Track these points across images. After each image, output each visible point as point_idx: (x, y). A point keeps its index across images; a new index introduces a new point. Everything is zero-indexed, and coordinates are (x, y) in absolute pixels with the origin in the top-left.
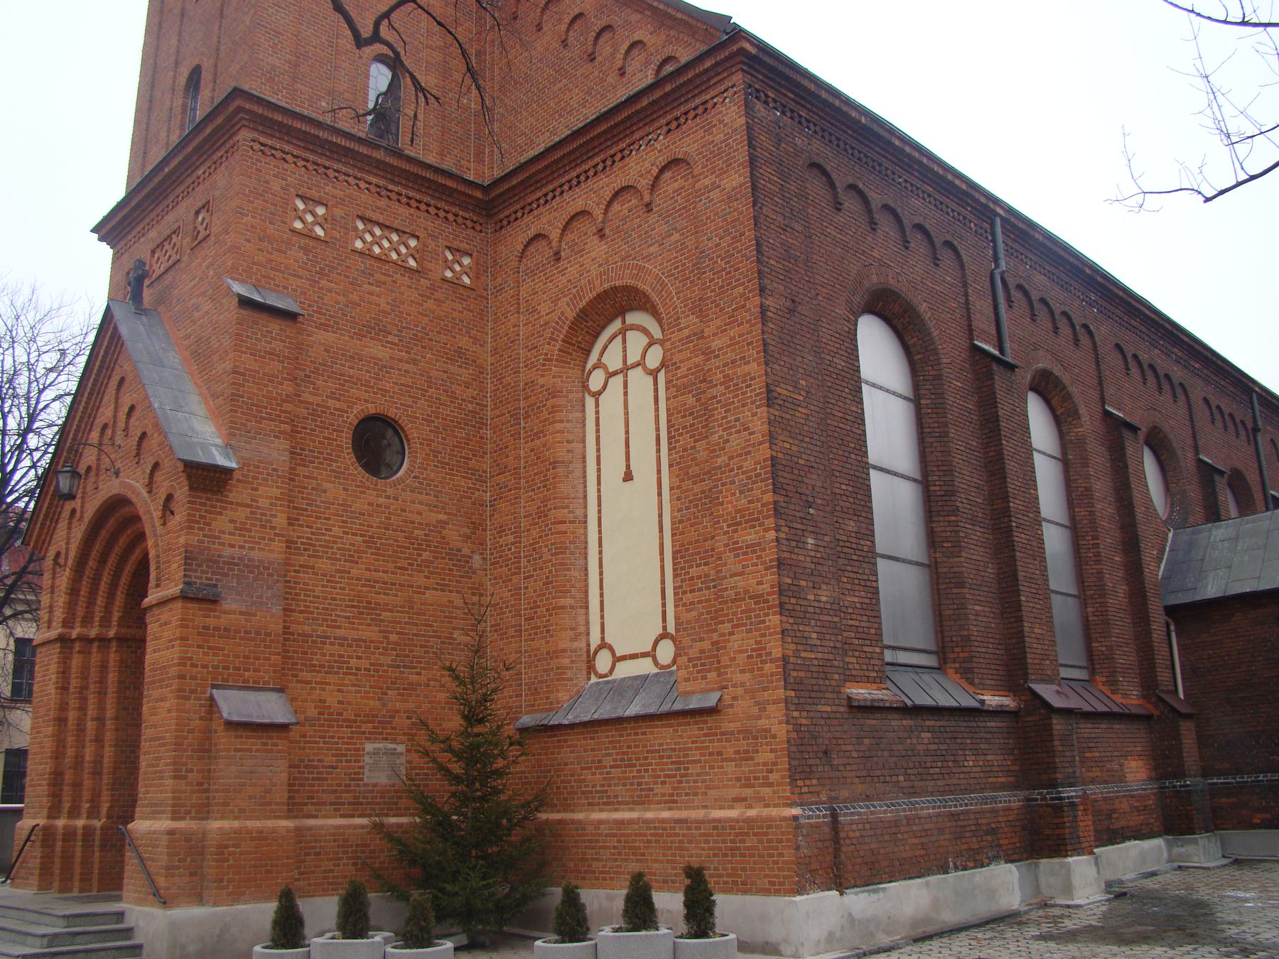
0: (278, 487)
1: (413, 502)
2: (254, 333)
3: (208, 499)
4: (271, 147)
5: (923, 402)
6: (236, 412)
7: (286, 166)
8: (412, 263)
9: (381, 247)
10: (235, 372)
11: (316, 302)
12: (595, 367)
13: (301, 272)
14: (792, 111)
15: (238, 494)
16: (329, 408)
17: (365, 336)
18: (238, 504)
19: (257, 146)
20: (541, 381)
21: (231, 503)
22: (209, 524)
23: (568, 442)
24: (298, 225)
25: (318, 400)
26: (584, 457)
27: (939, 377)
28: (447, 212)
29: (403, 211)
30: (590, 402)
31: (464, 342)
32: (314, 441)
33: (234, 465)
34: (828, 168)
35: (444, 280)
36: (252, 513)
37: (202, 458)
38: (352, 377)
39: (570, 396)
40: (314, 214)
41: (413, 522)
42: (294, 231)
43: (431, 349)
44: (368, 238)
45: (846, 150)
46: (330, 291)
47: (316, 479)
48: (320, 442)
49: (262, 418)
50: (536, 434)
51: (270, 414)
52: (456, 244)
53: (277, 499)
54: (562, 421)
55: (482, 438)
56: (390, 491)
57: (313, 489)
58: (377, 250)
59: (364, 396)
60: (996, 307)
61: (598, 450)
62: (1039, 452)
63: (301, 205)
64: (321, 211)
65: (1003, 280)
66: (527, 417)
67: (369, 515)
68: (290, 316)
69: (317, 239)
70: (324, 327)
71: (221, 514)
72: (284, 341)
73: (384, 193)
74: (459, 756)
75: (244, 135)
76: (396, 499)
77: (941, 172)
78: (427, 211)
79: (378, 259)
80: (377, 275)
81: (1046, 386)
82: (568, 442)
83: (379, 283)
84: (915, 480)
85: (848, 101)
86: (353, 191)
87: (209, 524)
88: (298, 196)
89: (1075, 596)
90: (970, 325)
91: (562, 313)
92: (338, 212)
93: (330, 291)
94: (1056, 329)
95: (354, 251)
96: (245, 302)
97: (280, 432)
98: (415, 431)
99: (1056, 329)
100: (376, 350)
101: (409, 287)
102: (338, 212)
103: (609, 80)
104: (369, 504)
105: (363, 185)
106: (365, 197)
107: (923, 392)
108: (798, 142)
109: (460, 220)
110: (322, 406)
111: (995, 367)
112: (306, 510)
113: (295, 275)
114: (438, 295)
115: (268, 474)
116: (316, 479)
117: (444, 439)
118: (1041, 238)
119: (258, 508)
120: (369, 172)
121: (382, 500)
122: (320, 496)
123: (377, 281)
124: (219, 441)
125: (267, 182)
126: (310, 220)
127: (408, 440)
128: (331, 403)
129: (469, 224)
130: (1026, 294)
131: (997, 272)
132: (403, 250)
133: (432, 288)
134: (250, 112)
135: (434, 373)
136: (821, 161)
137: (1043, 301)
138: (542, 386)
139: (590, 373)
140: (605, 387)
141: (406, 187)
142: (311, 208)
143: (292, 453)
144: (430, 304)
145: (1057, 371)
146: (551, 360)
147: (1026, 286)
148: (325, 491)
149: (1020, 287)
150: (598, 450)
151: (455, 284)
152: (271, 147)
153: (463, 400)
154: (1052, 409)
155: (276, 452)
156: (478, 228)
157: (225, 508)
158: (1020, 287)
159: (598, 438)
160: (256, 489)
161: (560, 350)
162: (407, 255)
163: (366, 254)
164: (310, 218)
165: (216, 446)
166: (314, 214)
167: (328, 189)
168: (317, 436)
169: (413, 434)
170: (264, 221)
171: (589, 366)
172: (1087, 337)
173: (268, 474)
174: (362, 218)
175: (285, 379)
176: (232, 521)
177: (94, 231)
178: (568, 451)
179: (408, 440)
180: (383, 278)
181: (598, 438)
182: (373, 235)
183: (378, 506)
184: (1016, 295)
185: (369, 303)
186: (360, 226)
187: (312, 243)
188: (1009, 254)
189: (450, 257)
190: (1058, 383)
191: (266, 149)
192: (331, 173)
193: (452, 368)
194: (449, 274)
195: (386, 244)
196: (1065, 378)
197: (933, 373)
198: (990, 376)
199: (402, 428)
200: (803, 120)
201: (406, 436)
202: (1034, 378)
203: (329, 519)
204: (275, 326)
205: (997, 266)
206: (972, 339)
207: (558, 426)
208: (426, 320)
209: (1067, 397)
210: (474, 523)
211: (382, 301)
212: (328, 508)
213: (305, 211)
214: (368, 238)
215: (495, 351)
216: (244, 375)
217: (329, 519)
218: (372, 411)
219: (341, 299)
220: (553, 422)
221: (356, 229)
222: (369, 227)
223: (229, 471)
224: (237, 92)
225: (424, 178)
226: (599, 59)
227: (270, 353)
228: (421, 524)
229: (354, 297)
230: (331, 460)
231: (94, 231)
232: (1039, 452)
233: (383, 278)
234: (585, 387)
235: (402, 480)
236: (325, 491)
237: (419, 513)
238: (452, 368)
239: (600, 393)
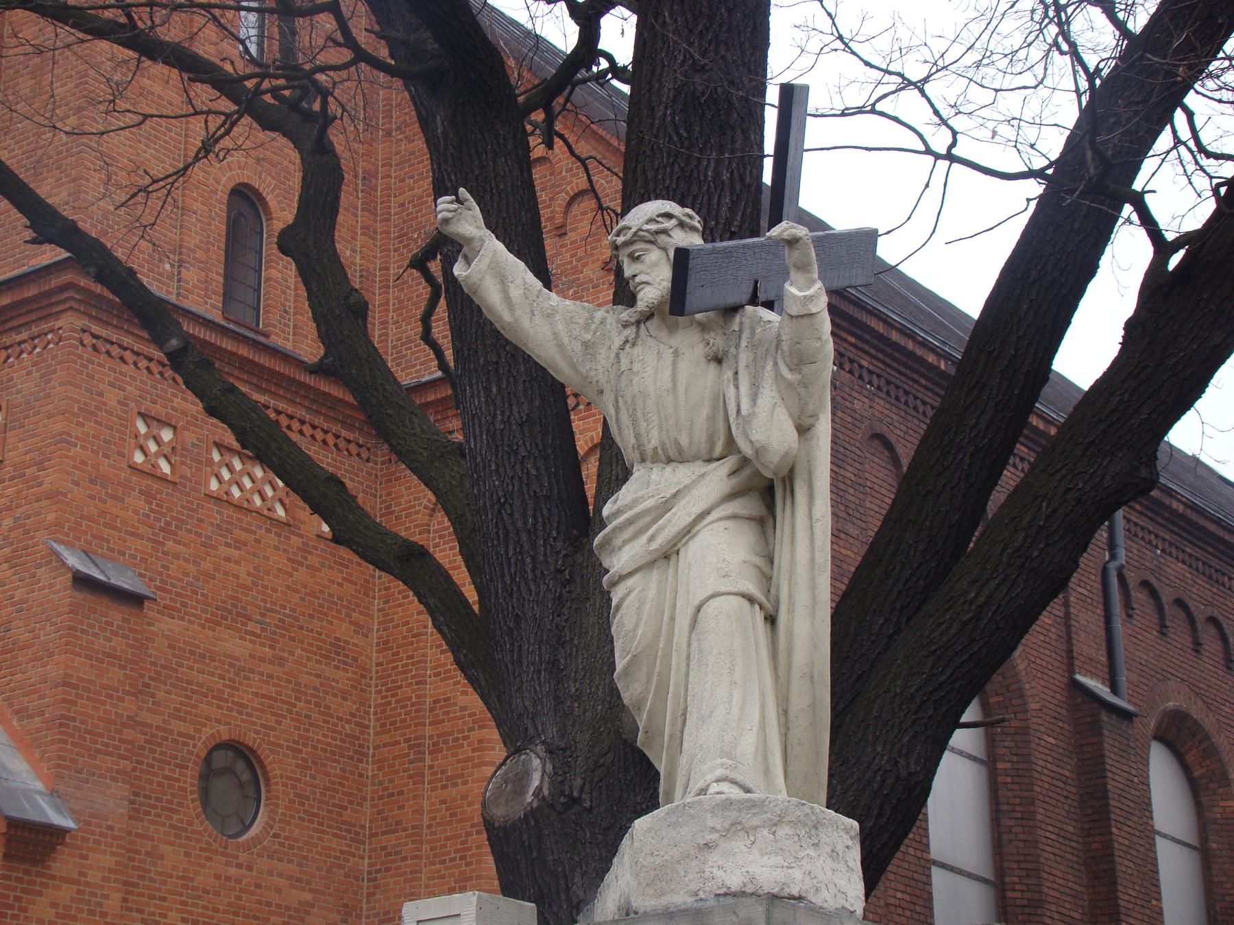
0: (112, 854)
1: (271, 873)
2: (92, 626)
3: (26, 872)
4: (106, 340)
5: (1000, 765)
6: (65, 742)
7: (124, 368)
9: (241, 488)
10: (65, 684)
11: (160, 574)
13: (142, 530)
14: (851, 361)
15: (63, 863)
16: (171, 732)
17: (219, 624)
18: (62, 879)
19: (88, 340)
21: (53, 877)
22: (24, 910)
24: (139, 458)
25: (156, 720)
27: (1024, 731)
28: (326, 432)
31: (343, 629)
32: (151, 782)
33: (68, 823)
34: (892, 439)
36: (79, 892)
37: (33, 816)
38: (200, 685)
40: (157, 440)
41: (268, 904)
42: (133, 468)
44: (226, 475)
45: (915, 408)
47: (152, 839)
48: (160, 784)
49: (98, 751)
50: (449, 778)
51: (107, 745)
53: (110, 871)
55: (361, 775)
56: (243, 857)
57: (147, 853)
58: (236, 493)
60: (1108, 619)
62: (1165, 836)
63: (142, 428)
64: (167, 435)
65: (1121, 577)
66: (436, 750)
67: (217, 893)
68: (135, 600)
69: (163, 479)
70: (167, 610)
71: (40, 894)
72: (127, 637)
76: (250, 868)
77: (1041, 426)
79: (238, 507)
80: (236, 532)
81: (1179, 735)
83: (239, 544)
84: (985, 881)
87: (24, 910)
88: (140, 414)
90: (1070, 651)
92: (189, 437)
94: (1197, 646)
95: (209, 496)
96: (82, 581)
97: (118, 772)
99: (1197, 646)
100: (234, 645)
101: (277, 548)
102: (189, 437)
103: (587, 272)
104: (217, 877)
107: (1001, 751)
108: (857, 405)
109: (342, 444)
110: (164, 730)
111: (1105, 717)
112: (136, 885)
113: (132, 534)
114: (313, 560)
115: (102, 834)
116: (152, 839)
118: (1181, 508)
119: (87, 884)
121: (232, 871)
122: (155, 864)
123: (237, 541)
124: (39, 785)
125: (101, 394)
126: (153, 449)
127: (267, 780)
128: (175, 725)
129: (354, 449)
130: (1154, 594)
131: (1113, 566)
133: (305, 550)
134: (84, 290)
136: (885, 430)
137: (1179, 602)
138: (463, 709)
141: (275, 395)
142: (155, 431)
143: (132, 802)
144: (301, 574)
145: (1196, 710)
147: (1155, 582)
148: (162, 857)
149: (1145, 584)
152: (106, 340)
154: (1186, 769)
155: (111, 800)
156: (365, 455)
157: (45, 886)
158: (1145, 584)
160: (85, 857)
163: (222, 500)
164: (153, 447)
165: (40, 793)
166: (157, 440)
168: (155, 774)
169: (275, 770)
170: (96, 452)
173: (102, 834)
175: (128, 693)
176: (54, 905)
179: (268, 785)
180: (244, 536)
182: (231, 469)
183: (228, 879)
184: (1139, 596)
185: (226, 573)
188: (1131, 535)
190: (1196, 729)
191: (99, 343)
196: (1209, 722)
197: (1017, 724)
198: (1096, 729)
199: (260, 761)
200: (865, 373)
201: (265, 773)
202: (1160, 723)
203: (164, 899)
204: (117, 614)
205: (1113, 557)
206: (1071, 672)
208: (296, 598)
209: (1211, 752)
210: (345, 906)
211: (242, 571)
212: (164, 882)
215: (384, 646)
216: (76, 687)
217: (164, 899)
218: (225, 737)
219: (192, 568)
221: (210, 462)
223: (55, 834)
225: (300, 383)
226: (571, 236)
227: (110, 656)
228: (279, 906)
229: (207, 565)
230: (171, 810)
232: (1165, 836)
233: (244, 536)
235: (257, 841)
236: (162, 857)
237: (278, 891)
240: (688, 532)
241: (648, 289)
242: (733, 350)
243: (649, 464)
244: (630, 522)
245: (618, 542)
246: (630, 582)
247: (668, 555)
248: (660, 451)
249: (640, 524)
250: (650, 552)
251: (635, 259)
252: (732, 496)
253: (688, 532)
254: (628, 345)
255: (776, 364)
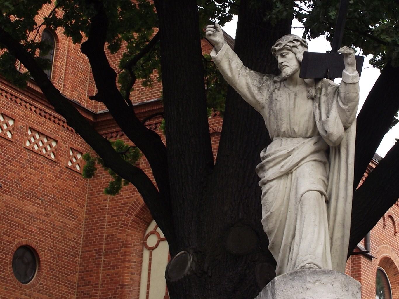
8: (53, 157)
12: (152, 233)
17: (25, 199)
20: (119, 236)
23: (132, 274)
26: (139, 284)
29: (52, 125)
30: (146, 253)
35: (67, 167)
39: (136, 248)
43: (57, 208)
44: (33, 140)
46: (11, 171)
50: (111, 266)
52: (75, 146)
54: (129, 261)
56: (28, 291)
58: (36, 147)
59: (21, 234)
61: (149, 281)
69: (8, 140)
73: (43, 114)
78: (63, 126)
79: (36, 153)
82: (132, 274)
83: (36, 168)
86: (28, 112)
91: (137, 200)
92: (20, 125)
93: (11, 171)
98: (45, 257)
101: (50, 171)
105: (33, 109)
106: (33, 116)
114: (63, 176)
117: (57, 262)
120: (37, 101)
123: (35, 167)
133: (61, 172)
135: (56, 223)
138: (119, 239)
139: (148, 236)
140: (157, 246)
144: (59, 181)
146: (127, 225)
150: (149, 281)
151: (72, 170)
153: (69, 240)
159: (149, 274)
161: (133, 221)
162: (7, 130)
163: (30, 150)
167: (16, 110)
169: (42, 258)
171: (148, 231)
174: (31, 129)
178: (131, 279)
180: (38, 165)
181: (149, 274)
182: (35, 139)
185: (30, 179)
186: (29, 133)
189: (71, 154)
192: (18, 101)
193: (66, 221)
194: (70, 164)
195: (41, 144)
207: (127, 264)
213: (72, 156)
218: (24, 244)
220: (125, 261)
221: (27, 135)
222: (34, 133)
229: (23, 175)
233: (38, 165)
234: (145, 244)
235: (34, 285)
238: (66, 221)
239: (153, 249)
240: (297, 165)
241: (287, 68)
242: (318, 95)
243: (280, 137)
244: (273, 159)
245: (267, 167)
246: (272, 183)
247: (288, 173)
248: (286, 132)
249: (277, 160)
250: (281, 172)
251: (283, 56)
252: (315, 152)
253: (297, 165)
254: (276, 90)
255: (337, 101)
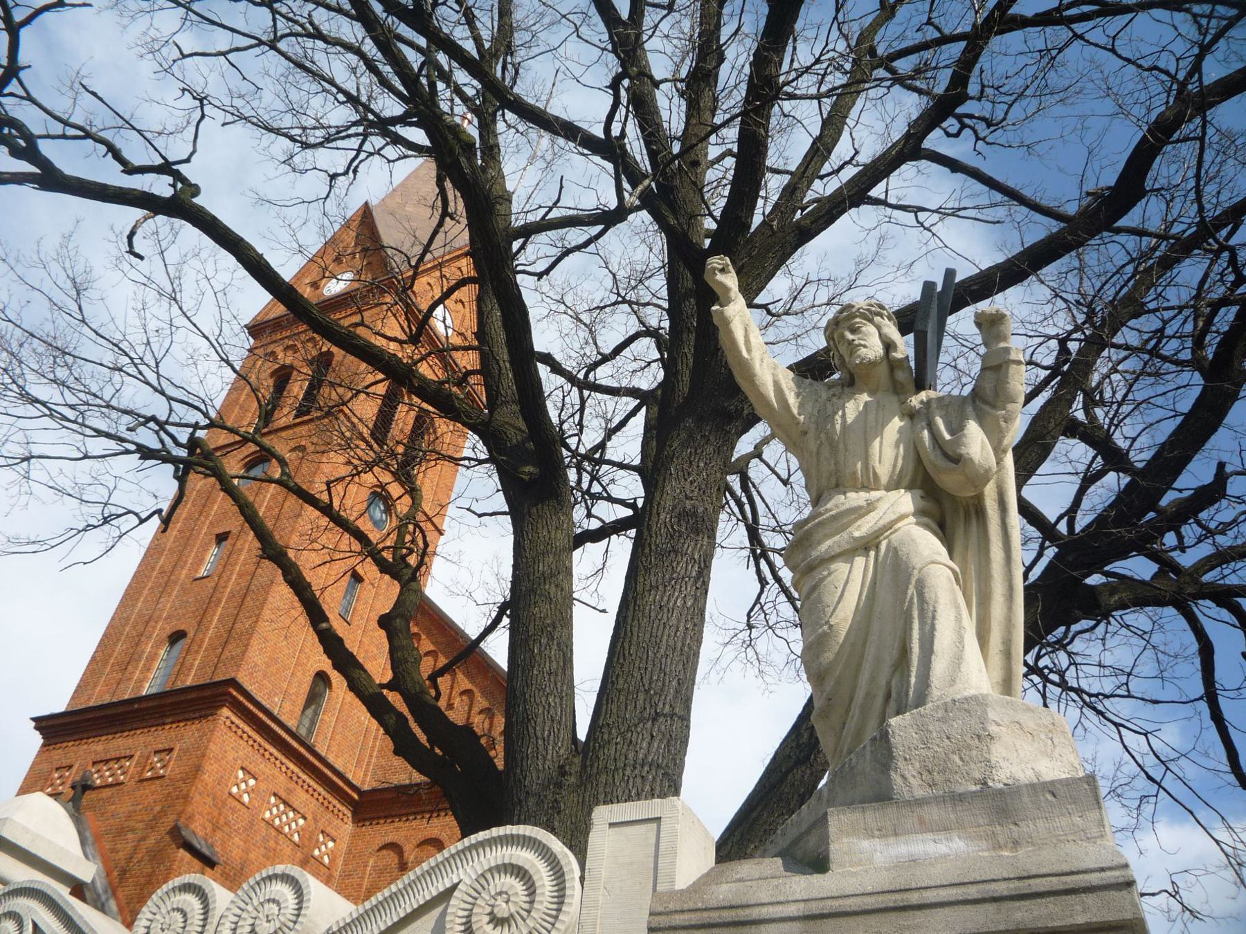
64: (252, 782)
74: (867, 556)
75: (226, 712)
85: (441, 611)
89: (1203, 219)
132: (293, 825)
163: (269, 824)
172: (581, 240)
177: (33, 719)
187: (239, 806)
214: (275, 811)
221: (269, 802)
224: (233, 682)
231: (33, 719)
